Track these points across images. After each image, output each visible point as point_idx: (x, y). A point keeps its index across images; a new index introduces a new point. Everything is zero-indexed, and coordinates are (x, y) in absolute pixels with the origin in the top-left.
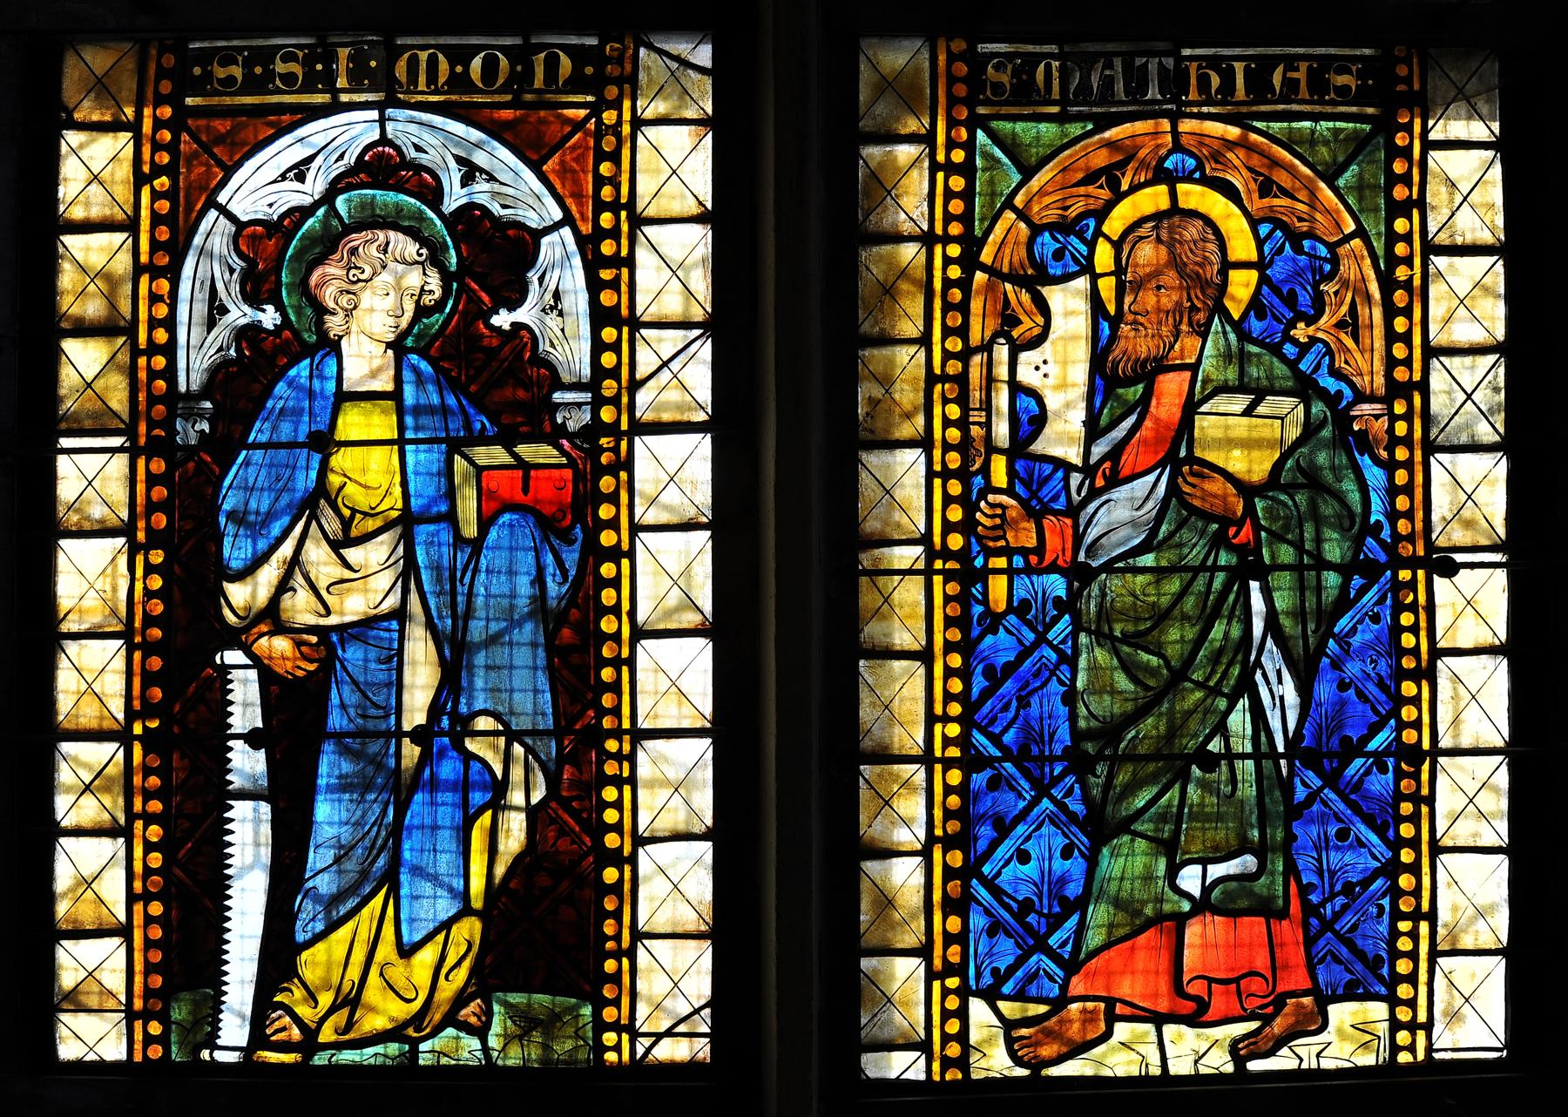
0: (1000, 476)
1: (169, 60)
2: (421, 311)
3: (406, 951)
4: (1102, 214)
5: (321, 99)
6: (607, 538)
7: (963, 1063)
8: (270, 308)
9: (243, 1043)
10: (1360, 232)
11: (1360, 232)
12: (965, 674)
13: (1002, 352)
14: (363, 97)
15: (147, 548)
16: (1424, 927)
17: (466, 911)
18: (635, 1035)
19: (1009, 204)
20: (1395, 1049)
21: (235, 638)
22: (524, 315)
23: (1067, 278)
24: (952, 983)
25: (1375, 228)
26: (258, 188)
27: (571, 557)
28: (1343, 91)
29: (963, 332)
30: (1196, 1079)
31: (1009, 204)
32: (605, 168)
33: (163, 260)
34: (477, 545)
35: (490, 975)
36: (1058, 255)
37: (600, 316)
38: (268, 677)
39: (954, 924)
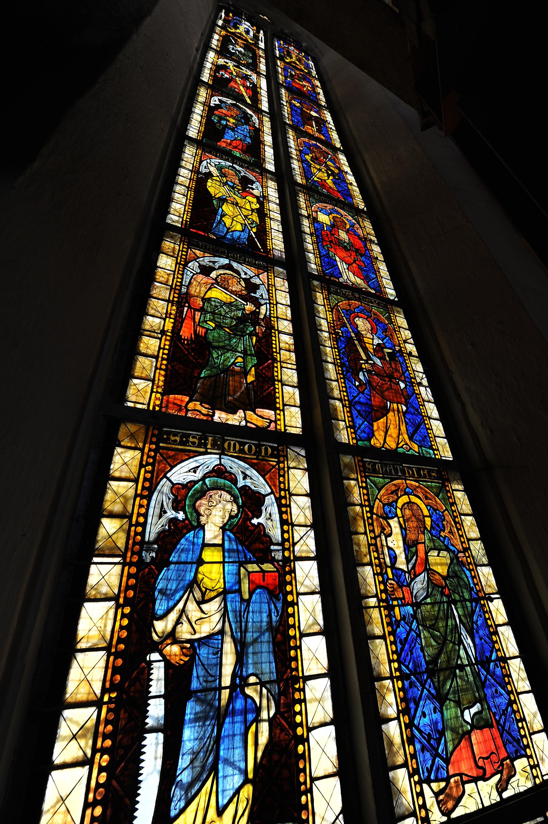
2: (231, 517)
3: (220, 812)
6: (290, 598)
8: (181, 513)
13: (383, 537)
15: (123, 606)
21: (156, 647)
25: (449, 509)
26: (181, 473)
32: (281, 479)
33: (146, 493)
37: (283, 522)
38: (168, 665)
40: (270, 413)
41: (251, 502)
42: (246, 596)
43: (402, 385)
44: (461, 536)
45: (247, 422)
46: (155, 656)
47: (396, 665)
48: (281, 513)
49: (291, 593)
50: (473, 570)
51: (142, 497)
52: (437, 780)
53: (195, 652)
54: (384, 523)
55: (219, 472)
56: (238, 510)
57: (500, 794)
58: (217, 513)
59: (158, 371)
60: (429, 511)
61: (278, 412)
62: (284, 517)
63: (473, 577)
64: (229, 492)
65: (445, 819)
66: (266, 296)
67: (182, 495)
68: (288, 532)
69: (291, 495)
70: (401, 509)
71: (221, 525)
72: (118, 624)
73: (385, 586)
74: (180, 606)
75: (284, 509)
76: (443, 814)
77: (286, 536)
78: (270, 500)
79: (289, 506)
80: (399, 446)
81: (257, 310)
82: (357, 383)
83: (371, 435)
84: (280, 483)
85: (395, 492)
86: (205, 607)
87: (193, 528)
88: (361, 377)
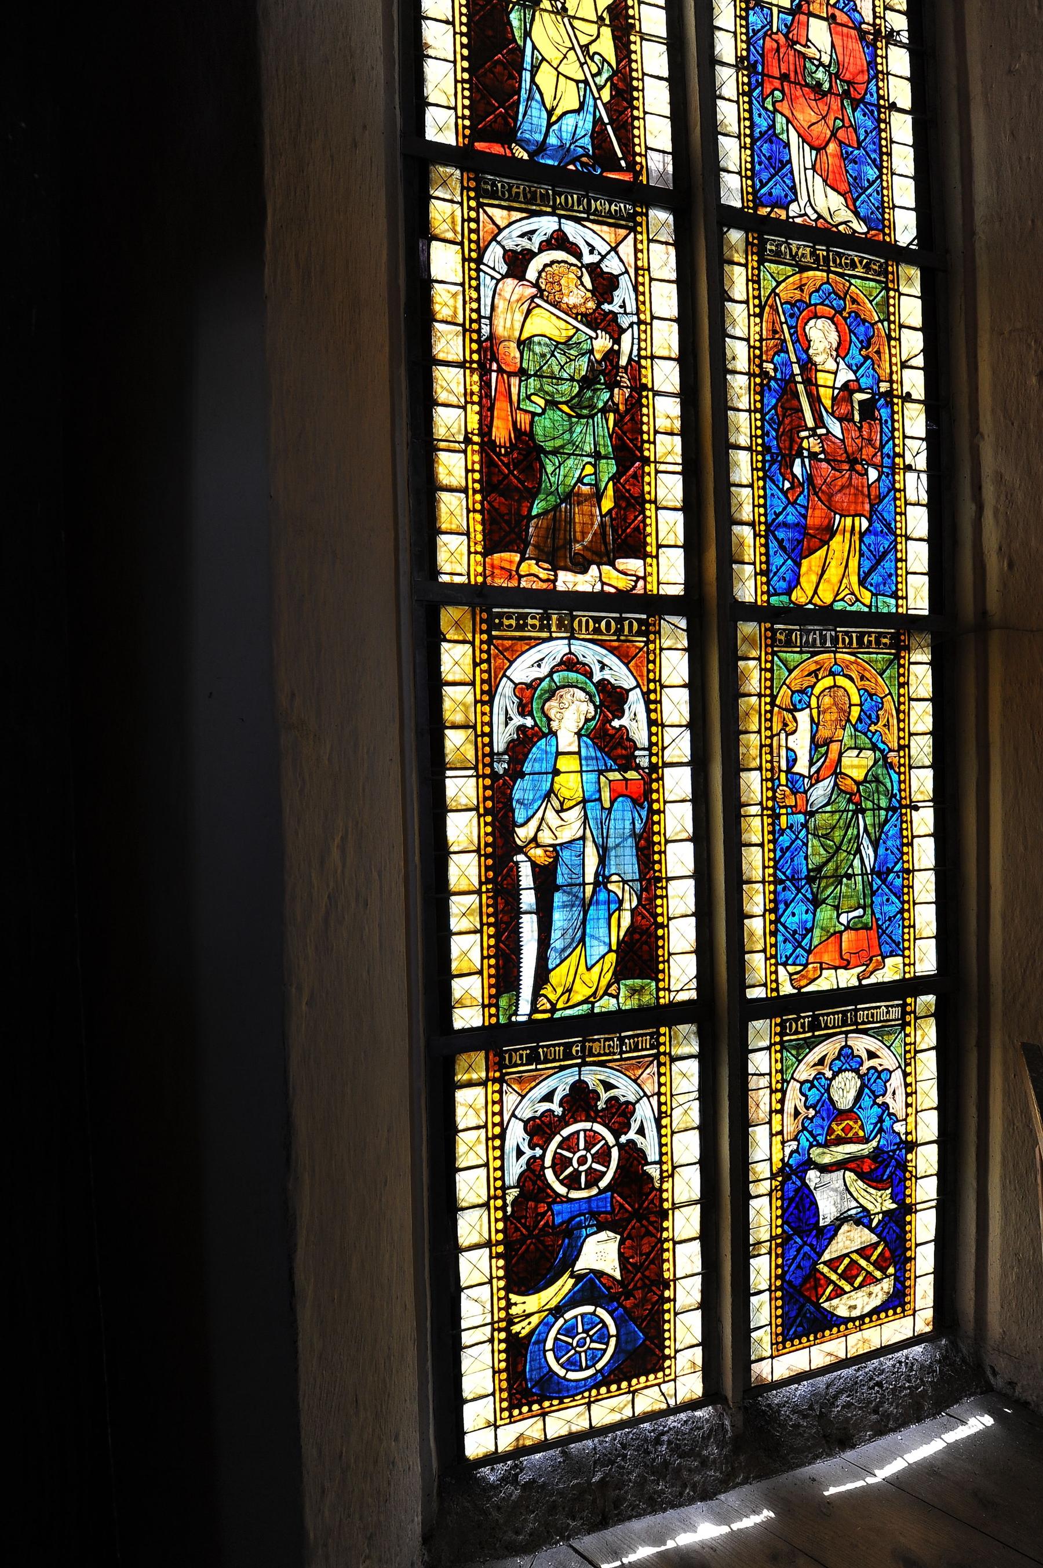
0: (783, 781)
2: (587, 720)
4: (813, 687)
6: (655, 806)
7: (777, 990)
8: (529, 718)
10: (890, 694)
13: (783, 735)
15: (484, 815)
17: (610, 950)
20: (905, 973)
23: (803, 709)
24: (773, 961)
25: (894, 692)
29: (771, 729)
32: (651, 666)
33: (486, 698)
34: (610, 810)
35: (620, 974)
36: (800, 701)
37: (651, 723)
38: (534, 865)
39: (773, 940)
40: (634, 565)
41: (611, 699)
45: (603, 583)
46: (520, 857)
48: (648, 711)
51: (483, 703)
54: (788, 716)
55: (570, 663)
57: (860, 980)
58: (571, 713)
61: (649, 560)
62: (653, 716)
64: (582, 689)
68: (656, 734)
69: (662, 687)
70: (818, 698)
73: (774, 792)
76: (794, 987)
81: (616, 347)
83: (795, 582)
84: (649, 671)
85: (815, 673)
87: (545, 735)
88: (797, 469)
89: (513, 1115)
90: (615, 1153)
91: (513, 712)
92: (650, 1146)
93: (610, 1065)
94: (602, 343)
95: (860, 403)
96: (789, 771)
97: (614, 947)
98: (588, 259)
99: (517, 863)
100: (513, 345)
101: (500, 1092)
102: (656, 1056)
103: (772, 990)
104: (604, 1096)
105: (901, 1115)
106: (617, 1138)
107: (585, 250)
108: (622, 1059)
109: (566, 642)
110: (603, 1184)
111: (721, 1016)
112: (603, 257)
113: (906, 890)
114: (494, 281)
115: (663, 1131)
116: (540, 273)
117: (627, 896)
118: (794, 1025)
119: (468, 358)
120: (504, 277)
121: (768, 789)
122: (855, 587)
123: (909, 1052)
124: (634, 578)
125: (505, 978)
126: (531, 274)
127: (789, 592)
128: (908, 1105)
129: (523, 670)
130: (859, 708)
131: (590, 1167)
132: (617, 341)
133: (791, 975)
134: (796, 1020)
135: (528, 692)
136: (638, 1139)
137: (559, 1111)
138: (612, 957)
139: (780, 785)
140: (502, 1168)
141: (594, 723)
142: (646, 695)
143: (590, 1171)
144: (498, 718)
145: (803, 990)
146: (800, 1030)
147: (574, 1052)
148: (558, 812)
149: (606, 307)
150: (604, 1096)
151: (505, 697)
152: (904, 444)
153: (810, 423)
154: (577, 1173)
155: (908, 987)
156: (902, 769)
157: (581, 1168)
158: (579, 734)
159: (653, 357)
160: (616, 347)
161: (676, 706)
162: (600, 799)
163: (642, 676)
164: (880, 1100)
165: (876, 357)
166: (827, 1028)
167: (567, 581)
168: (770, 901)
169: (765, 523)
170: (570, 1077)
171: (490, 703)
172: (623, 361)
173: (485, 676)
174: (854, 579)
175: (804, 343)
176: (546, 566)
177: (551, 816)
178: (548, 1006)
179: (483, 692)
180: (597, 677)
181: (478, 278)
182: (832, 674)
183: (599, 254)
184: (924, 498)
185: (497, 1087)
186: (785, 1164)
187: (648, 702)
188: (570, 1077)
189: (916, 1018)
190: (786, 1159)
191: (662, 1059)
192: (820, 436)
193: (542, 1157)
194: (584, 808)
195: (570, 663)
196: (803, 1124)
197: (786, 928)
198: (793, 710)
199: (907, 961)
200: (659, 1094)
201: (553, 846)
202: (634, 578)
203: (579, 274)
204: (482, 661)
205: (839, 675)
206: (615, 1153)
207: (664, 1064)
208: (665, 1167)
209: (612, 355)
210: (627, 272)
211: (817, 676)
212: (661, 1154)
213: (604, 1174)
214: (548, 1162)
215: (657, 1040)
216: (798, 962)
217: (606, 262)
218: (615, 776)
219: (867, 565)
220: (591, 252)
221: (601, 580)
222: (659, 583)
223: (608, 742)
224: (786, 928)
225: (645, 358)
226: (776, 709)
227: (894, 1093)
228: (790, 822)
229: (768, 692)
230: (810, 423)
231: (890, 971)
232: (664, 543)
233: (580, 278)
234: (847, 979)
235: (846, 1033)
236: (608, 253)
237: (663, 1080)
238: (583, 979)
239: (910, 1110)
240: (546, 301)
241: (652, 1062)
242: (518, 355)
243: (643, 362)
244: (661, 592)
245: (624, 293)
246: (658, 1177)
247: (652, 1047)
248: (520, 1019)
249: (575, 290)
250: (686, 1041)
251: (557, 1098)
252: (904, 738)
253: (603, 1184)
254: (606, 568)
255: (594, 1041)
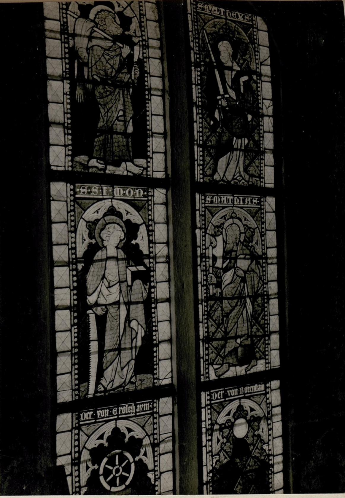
0: (211, 271)
1: (72, 187)
2: (121, 241)
3: (122, 369)
4: (223, 224)
5: (101, 197)
6: (152, 284)
7: (209, 377)
8: (94, 240)
9: (93, 393)
10: (258, 227)
11: (258, 227)
12: (207, 306)
13: (211, 248)
14: (108, 197)
15: (73, 290)
16: (64, 70)
17: (132, 359)
18: (159, 380)
19: (210, 222)
20: (266, 367)
21: (91, 307)
22: (137, 241)
23: (218, 235)
24: (207, 363)
25: (260, 227)
26: (90, 214)
27: (147, 287)
28: (255, 203)
29: (205, 245)
30: (241, 376)
31: (210, 222)
32: (150, 213)
33: (73, 229)
34: (131, 286)
35: (137, 371)
36: (218, 231)
37: (150, 242)
38: (96, 315)
39: (207, 352)
40: (142, 162)
41: (131, 229)
42: (130, 283)
43: (250, 117)
44: (263, 245)
45: (128, 171)
46: (89, 312)
47: (206, 317)
48: (149, 236)
49: (153, 281)
50: (265, 267)
51: (72, 232)
52: (216, 364)
53: (107, 310)
54: (213, 240)
55: (112, 211)
56: (125, 236)
57: (246, 372)
58: (113, 236)
59: (66, 136)
60: (245, 229)
61: (149, 160)
62: (151, 238)
63: (263, 271)
64: (118, 224)
65: (216, 378)
66: (138, 33)
67: (92, 225)
68: (152, 247)
69: (155, 223)
70: (226, 230)
71: (116, 245)
72: (72, 298)
73: (207, 277)
74: (99, 289)
75: (150, 233)
76: (216, 376)
77: (151, 250)
78: (143, 230)
79: (154, 231)
80: (235, 177)
81: (132, 52)
82: (212, 123)
83: (215, 170)
84: (149, 215)
85: (224, 217)
86: (110, 289)
87: (101, 248)
88: (217, 115)
89: (84, 447)
90: (133, 466)
91: (86, 237)
92: (149, 462)
93: (130, 419)
94: (126, 51)
95: (244, 82)
96: (213, 266)
97: (134, 357)
98: (117, 9)
99: (88, 314)
100: (85, 51)
101: (78, 434)
102: (152, 414)
103: (207, 377)
104: (128, 436)
105: (266, 440)
106: (134, 458)
107: (116, 5)
108: (136, 416)
109: (110, 200)
110: (128, 483)
111: (185, 392)
112: (125, 9)
113: (266, 326)
114: (74, 19)
115: (156, 454)
116: (96, 15)
117: (139, 331)
118: (216, 395)
119: (63, 56)
120: (79, 17)
121: (204, 275)
122: (242, 173)
123: (269, 407)
124: (142, 169)
125: (83, 375)
126: (92, 16)
127: (212, 175)
128: (269, 435)
129: (90, 214)
130: (244, 235)
131: (121, 474)
132: (132, 50)
133: (215, 370)
134: (217, 392)
135: (93, 226)
136: (144, 458)
137: (106, 445)
138: (133, 362)
139: (209, 273)
140: (79, 476)
141: (124, 241)
142: (147, 226)
143: (121, 476)
144: (79, 240)
145: (222, 377)
146: (219, 398)
147: (114, 413)
148: (107, 288)
149: (126, 33)
150: (128, 436)
151: (82, 228)
152: (263, 103)
153: (222, 93)
154: (115, 478)
155: (264, 377)
156: (264, 265)
157: (117, 475)
158: (117, 248)
159: (149, 58)
160: (132, 52)
161: (161, 232)
162: (126, 281)
163: (145, 218)
164: (256, 433)
165: (249, 60)
166: (231, 396)
167: (110, 169)
168: (206, 332)
169: (202, 140)
170: (111, 425)
171: (75, 232)
172: (136, 59)
173: (73, 218)
174: (242, 169)
175: (217, 53)
176: (102, 162)
177: (105, 291)
178: (102, 389)
179: (72, 226)
180: (125, 218)
181: (67, 18)
182: (232, 217)
183: (123, 7)
184: (271, 129)
185: (77, 431)
186: (214, 468)
187: (148, 231)
188: (111, 425)
189: (272, 390)
190: (214, 465)
191: (155, 415)
192: (226, 98)
193: (99, 469)
194: (120, 285)
195: (112, 211)
196: (221, 446)
197: (213, 346)
198: (214, 236)
199: (267, 361)
200: (153, 434)
201: (105, 305)
202: (142, 169)
203: (114, 16)
204: (71, 211)
205: (235, 218)
206: (133, 466)
207: (156, 418)
208: (156, 473)
209: (131, 56)
210: (136, 16)
211: (225, 219)
212: (155, 466)
213: (128, 477)
214: (101, 472)
215: (153, 405)
216: (218, 363)
217: (125, 11)
218: (134, 269)
219: (247, 162)
220: (119, 6)
221: (126, 169)
222: (153, 171)
223: (131, 253)
224: (213, 346)
225: (146, 58)
226: (207, 235)
227: (263, 429)
228: (214, 292)
229: (203, 226)
230: (222, 93)
231: (260, 366)
232: (155, 151)
233: (114, 18)
234: (241, 370)
235: (240, 399)
236: (127, 7)
237: (155, 426)
238: (118, 374)
239: (270, 438)
240: (99, 29)
241: (150, 417)
242: (87, 55)
243: (145, 60)
244: (154, 176)
245: (134, 25)
246: (154, 478)
247: (150, 409)
248: (90, 396)
249: (112, 24)
250: (166, 404)
251: (105, 437)
252: (264, 249)
253: (128, 483)
254: (129, 164)
255: (123, 406)
